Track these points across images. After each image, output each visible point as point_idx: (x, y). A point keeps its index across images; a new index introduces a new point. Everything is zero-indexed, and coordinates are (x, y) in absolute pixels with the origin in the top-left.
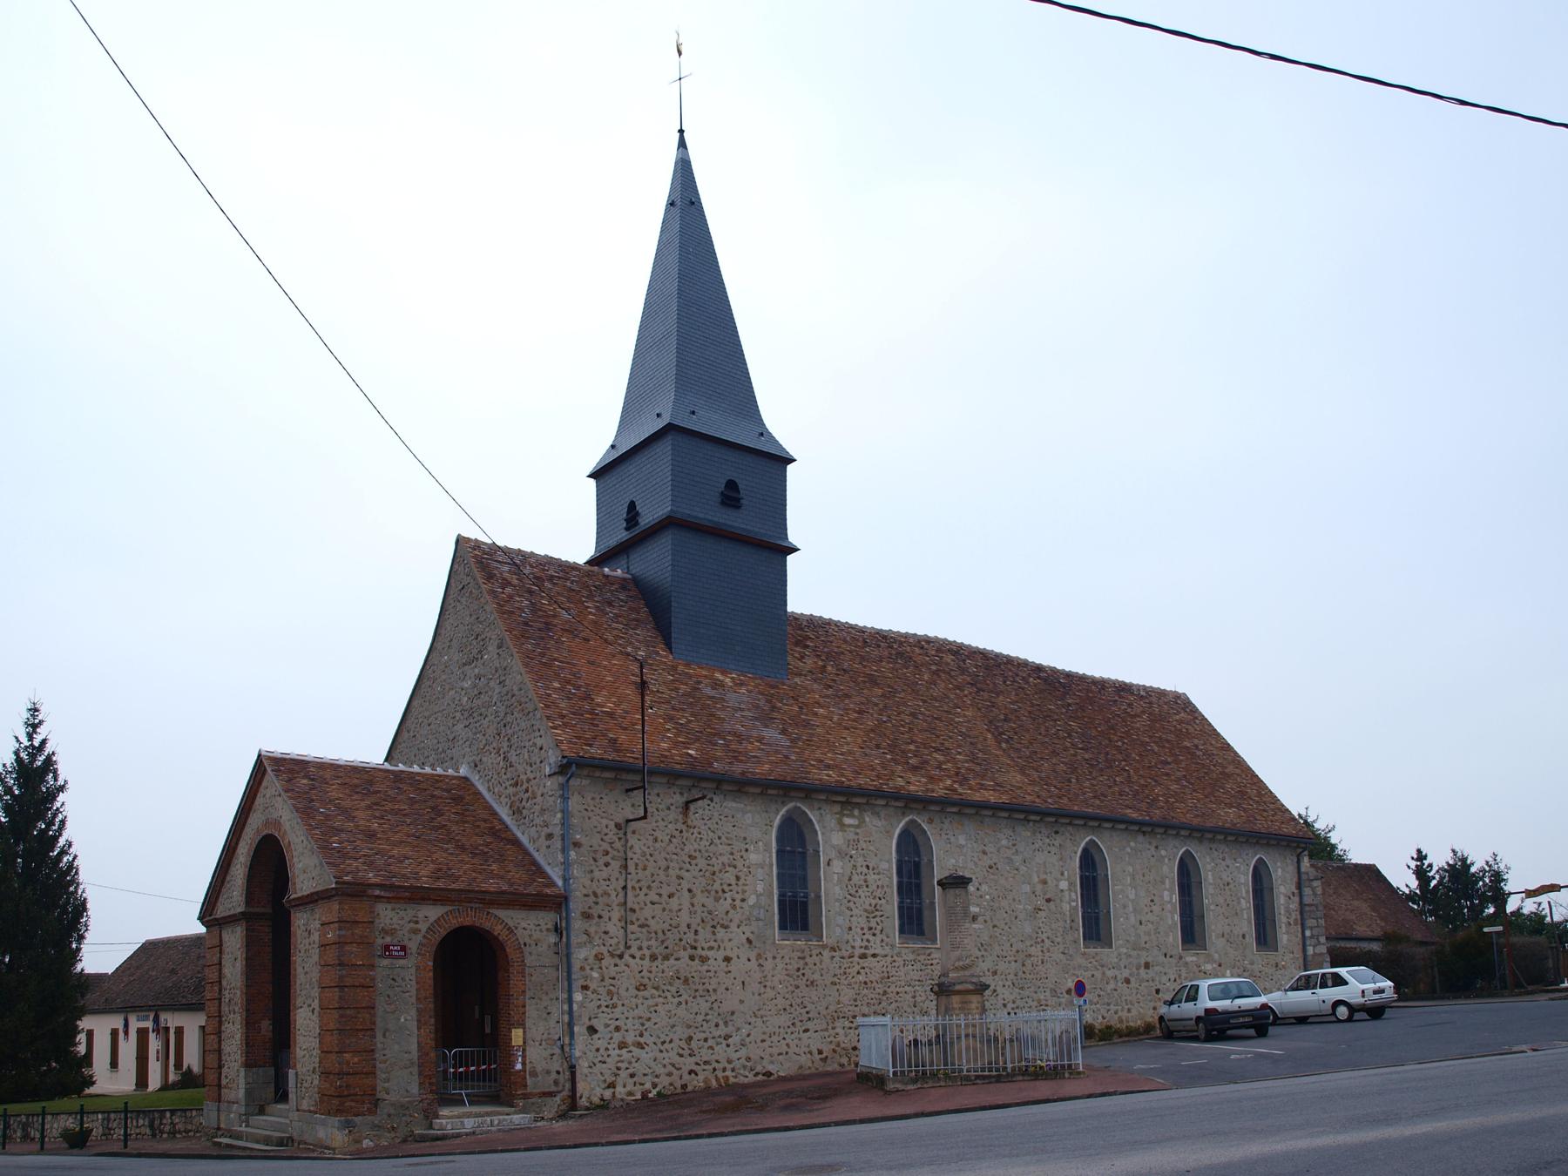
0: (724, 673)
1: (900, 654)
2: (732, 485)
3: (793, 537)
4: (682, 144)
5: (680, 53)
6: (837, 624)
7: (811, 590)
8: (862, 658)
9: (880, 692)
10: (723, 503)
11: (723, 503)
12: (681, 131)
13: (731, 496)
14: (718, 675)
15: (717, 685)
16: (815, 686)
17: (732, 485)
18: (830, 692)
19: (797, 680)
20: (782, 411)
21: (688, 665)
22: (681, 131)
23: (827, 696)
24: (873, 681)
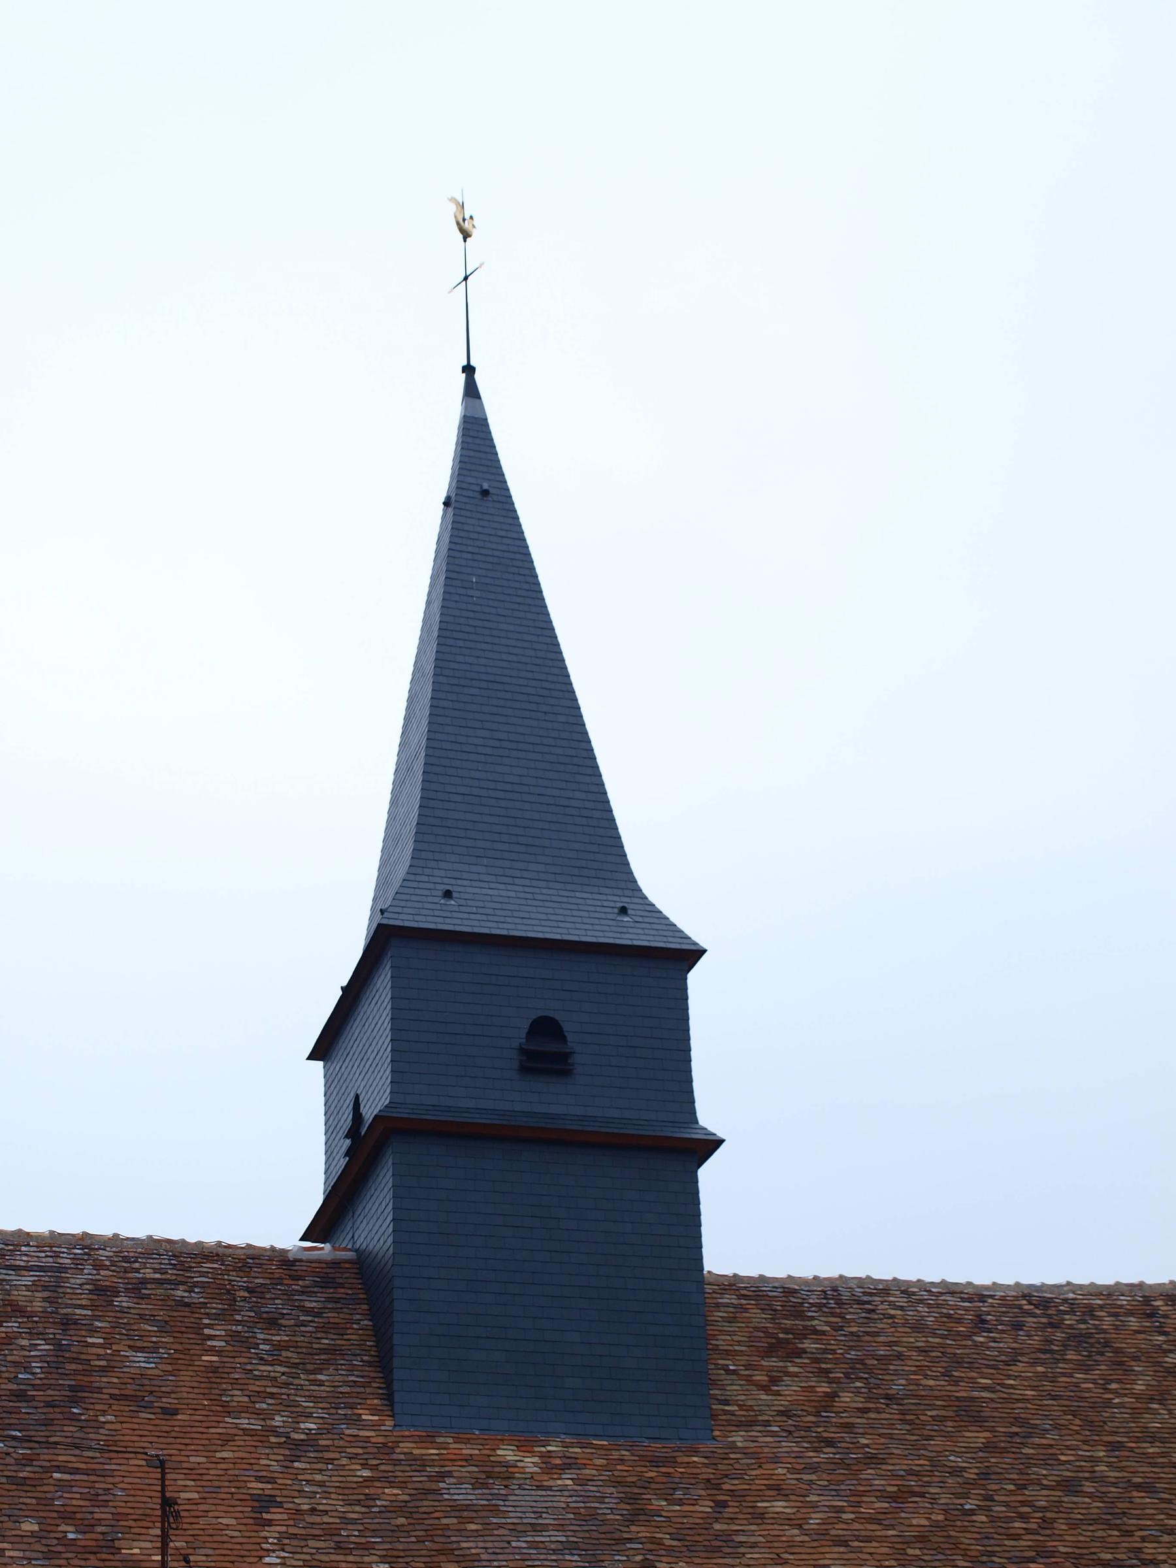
0: (524, 1446)
1: (1078, 1339)
2: (545, 1028)
3: (710, 1113)
4: (471, 391)
5: (466, 235)
6: (909, 1292)
7: (755, 1224)
8: (958, 1361)
9: (980, 1437)
10: (525, 1070)
11: (525, 1070)
12: (469, 370)
13: (546, 1051)
14: (507, 1453)
15: (494, 1474)
16: (787, 1445)
17: (546, 1027)
18: (828, 1453)
19: (738, 1438)
20: (673, 858)
21: (428, 1439)
22: (469, 370)
23: (813, 1468)
24: (968, 1413)
